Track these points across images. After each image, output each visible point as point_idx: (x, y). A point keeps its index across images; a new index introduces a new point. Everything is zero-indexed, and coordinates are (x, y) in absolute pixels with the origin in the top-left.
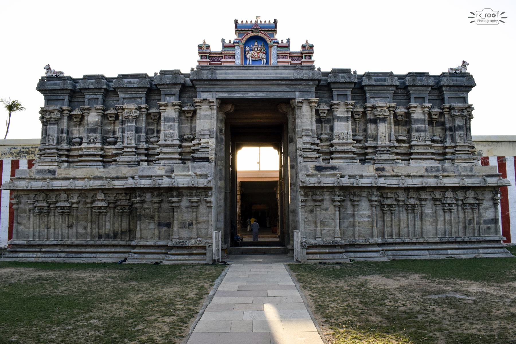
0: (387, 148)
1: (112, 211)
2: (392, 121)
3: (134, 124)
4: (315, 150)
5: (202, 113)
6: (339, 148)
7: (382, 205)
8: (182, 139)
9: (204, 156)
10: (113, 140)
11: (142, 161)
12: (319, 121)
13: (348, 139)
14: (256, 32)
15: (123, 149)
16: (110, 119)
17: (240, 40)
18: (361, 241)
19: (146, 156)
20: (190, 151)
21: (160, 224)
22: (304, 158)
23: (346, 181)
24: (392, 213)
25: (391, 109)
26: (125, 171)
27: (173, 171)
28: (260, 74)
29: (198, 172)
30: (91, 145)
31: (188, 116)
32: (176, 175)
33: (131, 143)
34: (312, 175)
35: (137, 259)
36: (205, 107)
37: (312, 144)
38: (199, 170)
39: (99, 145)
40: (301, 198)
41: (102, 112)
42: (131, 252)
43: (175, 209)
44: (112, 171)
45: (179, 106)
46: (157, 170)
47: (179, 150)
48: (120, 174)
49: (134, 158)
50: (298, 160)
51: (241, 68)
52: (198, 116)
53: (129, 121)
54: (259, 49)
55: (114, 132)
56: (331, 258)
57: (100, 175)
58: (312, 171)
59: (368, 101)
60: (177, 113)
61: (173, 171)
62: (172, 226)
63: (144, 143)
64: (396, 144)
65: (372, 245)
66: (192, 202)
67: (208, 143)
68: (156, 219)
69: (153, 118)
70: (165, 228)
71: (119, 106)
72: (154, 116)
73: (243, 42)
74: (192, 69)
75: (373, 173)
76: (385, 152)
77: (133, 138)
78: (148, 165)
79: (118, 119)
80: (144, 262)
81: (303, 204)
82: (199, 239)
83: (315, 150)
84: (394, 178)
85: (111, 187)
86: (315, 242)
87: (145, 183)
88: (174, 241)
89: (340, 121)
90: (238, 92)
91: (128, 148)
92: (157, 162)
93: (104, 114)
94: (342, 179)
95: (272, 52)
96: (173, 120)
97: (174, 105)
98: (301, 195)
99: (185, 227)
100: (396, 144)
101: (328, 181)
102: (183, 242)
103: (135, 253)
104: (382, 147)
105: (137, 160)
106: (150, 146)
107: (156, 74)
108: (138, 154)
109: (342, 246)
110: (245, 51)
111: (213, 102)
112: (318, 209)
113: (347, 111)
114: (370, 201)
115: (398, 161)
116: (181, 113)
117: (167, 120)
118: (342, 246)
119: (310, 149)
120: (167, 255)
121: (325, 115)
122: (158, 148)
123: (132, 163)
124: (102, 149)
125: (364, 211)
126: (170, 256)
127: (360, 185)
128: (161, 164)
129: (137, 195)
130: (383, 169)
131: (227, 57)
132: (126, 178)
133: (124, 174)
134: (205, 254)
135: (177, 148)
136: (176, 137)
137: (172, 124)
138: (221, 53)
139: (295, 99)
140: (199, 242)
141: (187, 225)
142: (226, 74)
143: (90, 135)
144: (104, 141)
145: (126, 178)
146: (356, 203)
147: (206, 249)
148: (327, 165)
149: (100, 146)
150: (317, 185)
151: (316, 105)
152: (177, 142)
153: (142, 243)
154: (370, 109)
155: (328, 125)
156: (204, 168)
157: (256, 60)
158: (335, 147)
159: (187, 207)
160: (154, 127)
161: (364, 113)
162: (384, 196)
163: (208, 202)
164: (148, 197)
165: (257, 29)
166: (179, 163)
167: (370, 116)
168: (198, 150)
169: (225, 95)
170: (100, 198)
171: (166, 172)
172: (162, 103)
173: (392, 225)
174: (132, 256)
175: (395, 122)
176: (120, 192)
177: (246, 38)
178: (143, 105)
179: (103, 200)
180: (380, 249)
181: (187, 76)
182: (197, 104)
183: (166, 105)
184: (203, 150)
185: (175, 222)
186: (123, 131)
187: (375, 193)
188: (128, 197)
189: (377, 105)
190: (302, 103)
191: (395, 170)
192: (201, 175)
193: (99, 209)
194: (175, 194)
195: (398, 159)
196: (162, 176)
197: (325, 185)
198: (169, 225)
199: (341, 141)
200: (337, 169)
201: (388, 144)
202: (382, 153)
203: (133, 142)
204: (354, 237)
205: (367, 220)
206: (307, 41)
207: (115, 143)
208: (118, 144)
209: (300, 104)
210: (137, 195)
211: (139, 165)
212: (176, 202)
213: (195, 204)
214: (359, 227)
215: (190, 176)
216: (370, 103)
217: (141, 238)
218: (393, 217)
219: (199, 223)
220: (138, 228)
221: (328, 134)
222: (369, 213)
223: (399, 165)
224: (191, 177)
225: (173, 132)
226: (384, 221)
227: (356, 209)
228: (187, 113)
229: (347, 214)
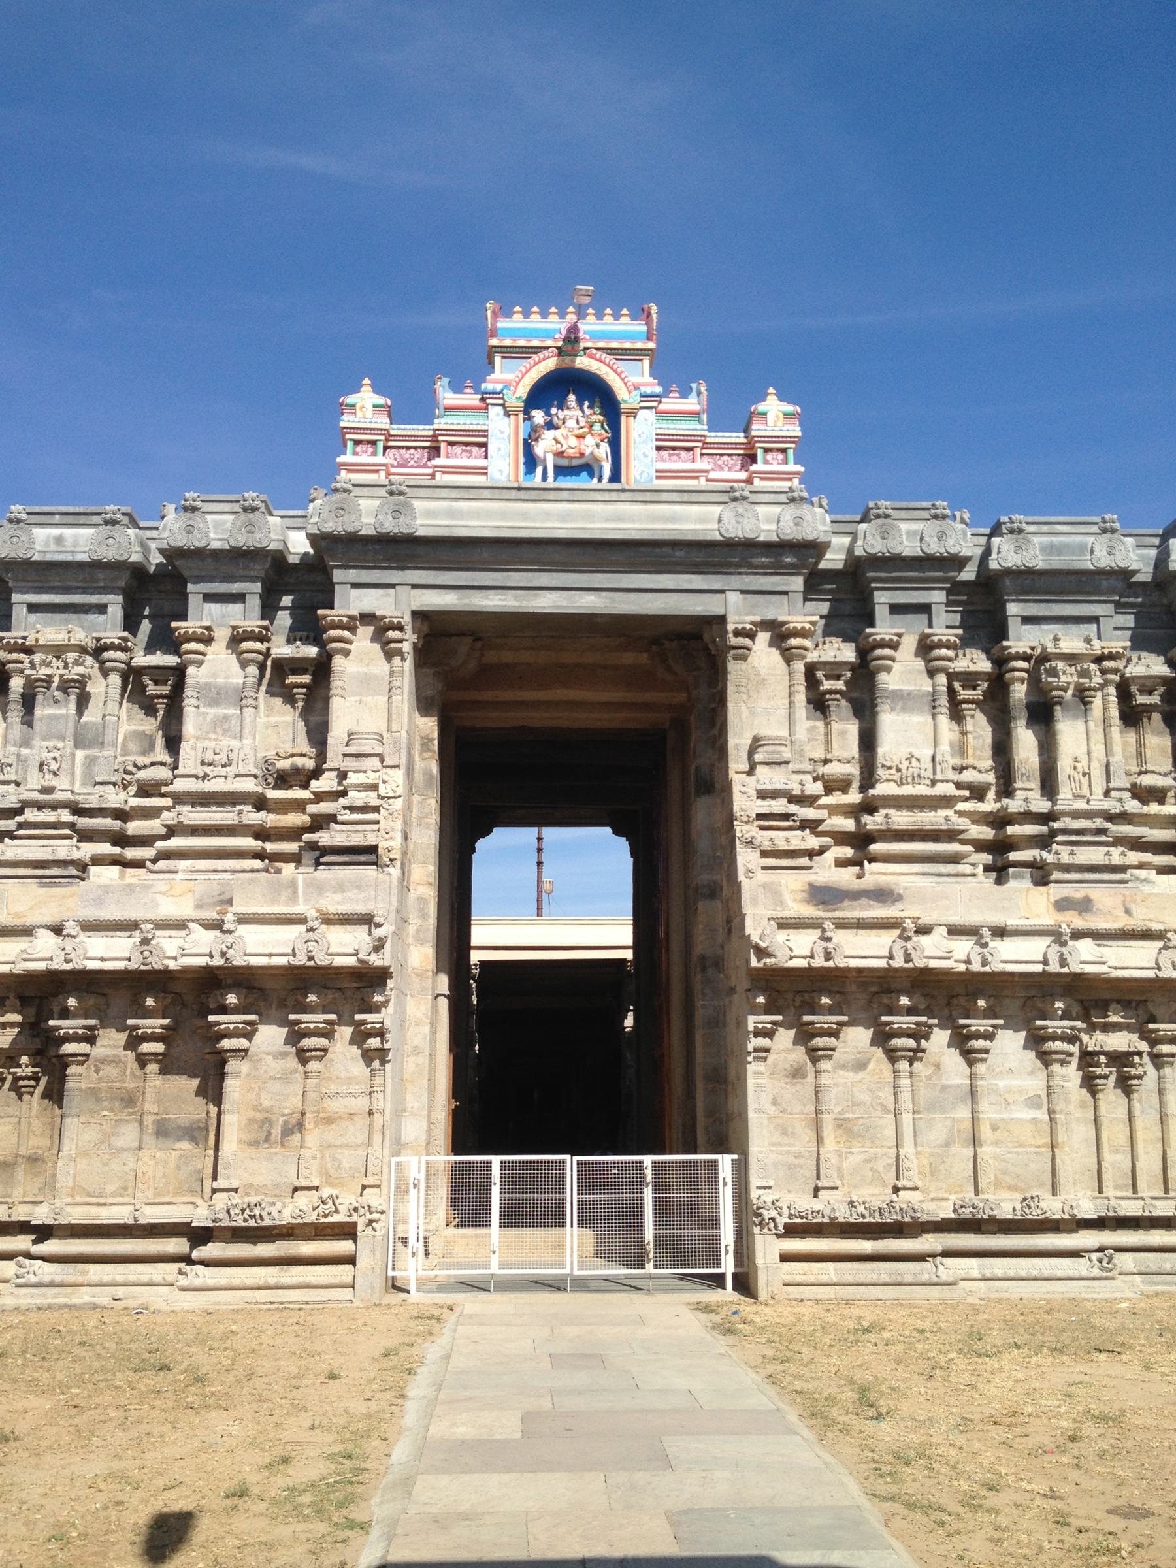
2: (1114, 713)
4: (805, 824)
6: (901, 819)
9: (356, 840)
11: (97, 860)
13: (934, 783)
15: (20, 811)
28: (589, 516)
29: (336, 904)
31: (307, 687)
35: (52, 1284)
36: (362, 641)
37: (793, 799)
38: (338, 897)
42: (29, 1256)
46: (161, 899)
50: (739, 859)
51: (514, 494)
56: (885, 1278)
59: (1011, 634)
61: (230, 902)
64: (1133, 806)
75: (1047, 918)
80: (84, 1296)
83: (805, 824)
84: (1132, 943)
86: (817, 1205)
88: (221, 1200)
89: (903, 709)
94: (924, 940)
99: (266, 1140)
100: (1133, 806)
104: (1076, 815)
115: (1142, 873)
119: (786, 817)
122: (168, 809)
126: (199, 1268)
132: (27, 932)
133: (17, 915)
134: (351, 1260)
141: (277, 1131)
142: (451, 514)
145: (27, 932)
148: (857, 885)
156: (359, 887)
168: (333, 818)
171: (199, 906)
190: (751, 635)
191: (1134, 908)
192: (346, 920)
195: (1141, 866)
196: (180, 925)
199: (907, 790)
200: (899, 898)
201: (1099, 803)
205: (1028, 1114)
209: (741, 641)
214: (996, 1143)
215: (300, 920)
216: (1019, 639)
223: (1146, 889)
225: (234, 743)
227: (980, 1068)
229: (944, 1088)
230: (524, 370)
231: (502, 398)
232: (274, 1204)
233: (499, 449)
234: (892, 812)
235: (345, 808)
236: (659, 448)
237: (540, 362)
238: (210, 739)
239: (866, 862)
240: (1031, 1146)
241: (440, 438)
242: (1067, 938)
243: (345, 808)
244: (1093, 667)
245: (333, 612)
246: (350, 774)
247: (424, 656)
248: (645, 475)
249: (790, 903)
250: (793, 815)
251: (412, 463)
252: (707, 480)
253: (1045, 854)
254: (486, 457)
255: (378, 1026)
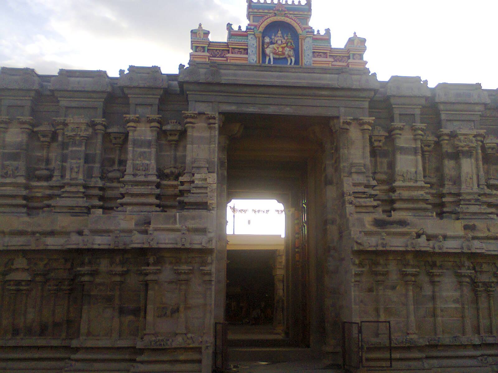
0: (476, 196)
1: (40, 288)
2: (480, 156)
3: (83, 148)
4: (371, 196)
5: (196, 134)
6: (406, 194)
7: (474, 283)
8: (161, 175)
10: (45, 172)
11: (94, 207)
12: (374, 153)
13: (416, 181)
14: (280, 15)
15: (63, 187)
16: (42, 139)
17: (255, 26)
18: (447, 339)
19: (100, 200)
20: (173, 193)
21: (122, 311)
22: (356, 206)
23: (423, 244)
24: (489, 296)
25: (479, 138)
26: (64, 222)
27: (149, 223)
30: (8, 180)
32: (156, 230)
33: (76, 179)
34: (368, 234)
36: (201, 124)
37: (366, 186)
38: (193, 222)
39: (22, 180)
40: (354, 269)
41: (30, 127)
42: (69, 359)
43: (150, 286)
44: (42, 221)
45: (159, 122)
47: (158, 191)
48: (57, 228)
49: (82, 202)
52: (189, 139)
53: (74, 144)
54: (284, 41)
55: (48, 161)
57: (21, 228)
58: (369, 227)
60: (155, 133)
62: (142, 314)
63: (99, 179)
64: (488, 191)
65: (465, 346)
66: (180, 274)
67: (206, 180)
68: (117, 301)
69: (114, 141)
70: (131, 317)
71: (61, 119)
72: (115, 138)
73: (261, 29)
74: (181, 66)
75: (461, 233)
76: (473, 202)
77: (81, 170)
78: (103, 213)
79: (57, 140)
81: (358, 279)
82: (189, 335)
83: (371, 196)
85: (41, 247)
87: (100, 242)
90: (254, 104)
91: (71, 185)
92: (119, 209)
93: (33, 131)
94: (419, 240)
95: (304, 47)
96: (149, 144)
97: (150, 121)
98: (354, 264)
100: (488, 191)
101: (397, 243)
102: (162, 340)
103: (77, 360)
104: (469, 194)
105: (86, 205)
106: (108, 184)
107: (121, 72)
108: (88, 196)
109: (421, 349)
110: (263, 43)
111: (214, 118)
112: (381, 288)
113: (415, 140)
114: (459, 275)
115: (492, 216)
116: (162, 133)
117: (137, 144)
118: (421, 349)
120: (135, 364)
121: (381, 144)
123: (77, 210)
124: (27, 187)
125: (449, 291)
126: (139, 365)
127: (445, 250)
128: (127, 213)
129: (87, 260)
130: (473, 228)
131: (236, 50)
132: (68, 234)
133: (63, 227)
135: (154, 187)
136: (153, 170)
137: (146, 150)
138: (227, 44)
139: (338, 118)
140: (190, 341)
141: (168, 312)
142: (235, 75)
143: (7, 163)
144: (31, 175)
146: (437, 279)
147: (200, 352)
149: (24, 181)
150: (380, 248)
151: (370, 128)
152: (154, 178)
153: (90, 343)
154: (447, 138)
155: (385, 160)
157: (281, 59)
158: (398, 192)
159: (171, 282)
160: (115, 156)
161: (438, 144)
162: (478, 269)
163: (205, 274)
164: (104, 265)
165: (282, 10)
166: (156, 211)
167: (447, 148)
168: (189, 191)
169: (233, 108)
170: (19, 266)
171: (136, 225)
172: (132, 116)
173: (490, 315)
174: (71, 365)
175: (483, 158)
176: (55, 257)
177: (266, 23)
178: (99, 120)
179: (24, 270)
180: (478, 353)
181: (171, 77)
182: (188, 120)
183: (138, 121)
184: (198, 191)
185: (150, 307)
186: (64, 159)
187: (467, 264)
188: (69, 266)
189: (458, 132)
191: (491, 229)
193: (16, 285)
194: (151, 260)
195: (491, 213)
196: (130, 231)
197: (393, 249)
198: (139, 311)
200: (408, 224)
201: (475, 189)
202: (469, 202)
203: (81, 177)
204: (436, 334)
205: (454, 306)
206: (355, 33)
207: (49, 178)
208: (54, 179)
209: (346, 126)
210: (87, 260)
211: (88, 213)
212: (185, 273)
213: (183, 277)
217: (89, 334)
218: (492, 302)
219: (189, 308)
220: (84, 316)
221: (386, 173)
222: (457, 294)
224: (178, 233)
226: (478, 309)
228: (170, 135)
230: (262, 21)
231: (254, 32)
232: (168, 340)
233: (253, 51)
234: (401, 192)
235: (194, 187)
236: (314, 52)
237: (268, 18)
238: (138, 161)
239: (392, 211)
240: (456, 317)
241: (229, 46)
242: (470, 239)
243: (194, 187)
244: (474, 139)
245: (189, 112)
246: (195, 175)
247: (222, 130)
248: (308, 62)
249: (368, 226)
250: (366, 192)
251: (218, 56)
252: (332, 65)
253: (457, 208)
254: (247, 54)
255: (209, 272)
